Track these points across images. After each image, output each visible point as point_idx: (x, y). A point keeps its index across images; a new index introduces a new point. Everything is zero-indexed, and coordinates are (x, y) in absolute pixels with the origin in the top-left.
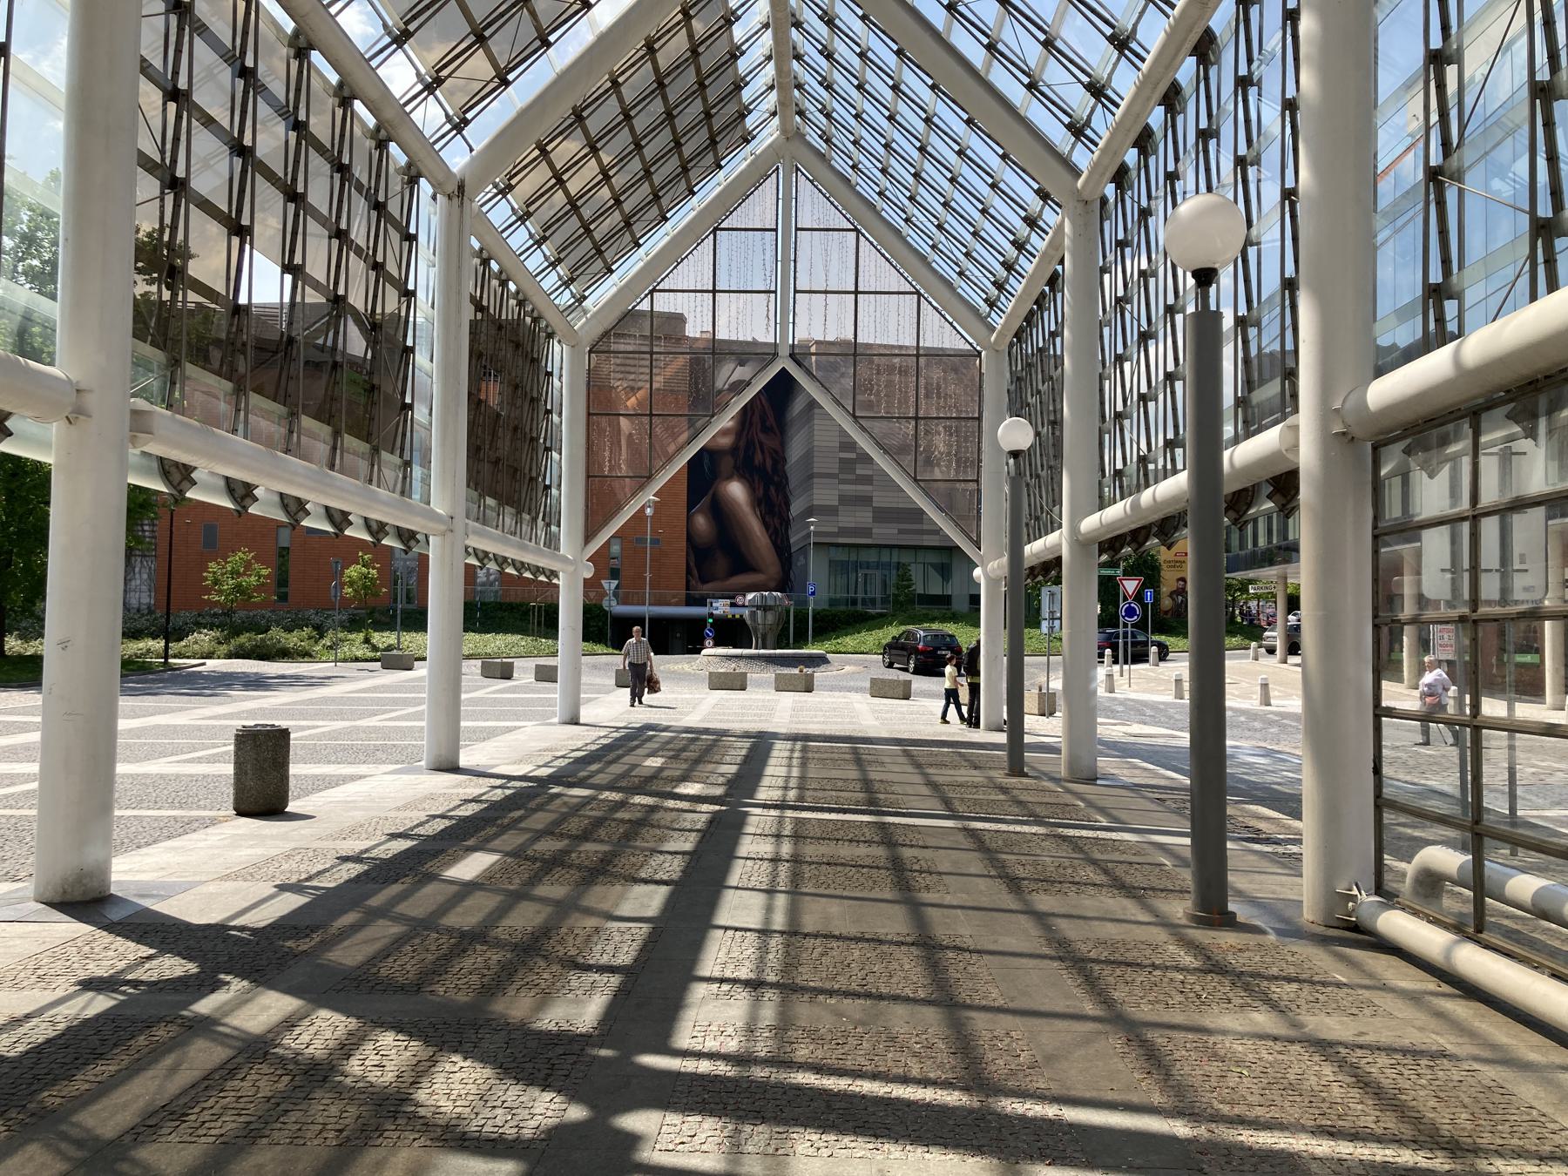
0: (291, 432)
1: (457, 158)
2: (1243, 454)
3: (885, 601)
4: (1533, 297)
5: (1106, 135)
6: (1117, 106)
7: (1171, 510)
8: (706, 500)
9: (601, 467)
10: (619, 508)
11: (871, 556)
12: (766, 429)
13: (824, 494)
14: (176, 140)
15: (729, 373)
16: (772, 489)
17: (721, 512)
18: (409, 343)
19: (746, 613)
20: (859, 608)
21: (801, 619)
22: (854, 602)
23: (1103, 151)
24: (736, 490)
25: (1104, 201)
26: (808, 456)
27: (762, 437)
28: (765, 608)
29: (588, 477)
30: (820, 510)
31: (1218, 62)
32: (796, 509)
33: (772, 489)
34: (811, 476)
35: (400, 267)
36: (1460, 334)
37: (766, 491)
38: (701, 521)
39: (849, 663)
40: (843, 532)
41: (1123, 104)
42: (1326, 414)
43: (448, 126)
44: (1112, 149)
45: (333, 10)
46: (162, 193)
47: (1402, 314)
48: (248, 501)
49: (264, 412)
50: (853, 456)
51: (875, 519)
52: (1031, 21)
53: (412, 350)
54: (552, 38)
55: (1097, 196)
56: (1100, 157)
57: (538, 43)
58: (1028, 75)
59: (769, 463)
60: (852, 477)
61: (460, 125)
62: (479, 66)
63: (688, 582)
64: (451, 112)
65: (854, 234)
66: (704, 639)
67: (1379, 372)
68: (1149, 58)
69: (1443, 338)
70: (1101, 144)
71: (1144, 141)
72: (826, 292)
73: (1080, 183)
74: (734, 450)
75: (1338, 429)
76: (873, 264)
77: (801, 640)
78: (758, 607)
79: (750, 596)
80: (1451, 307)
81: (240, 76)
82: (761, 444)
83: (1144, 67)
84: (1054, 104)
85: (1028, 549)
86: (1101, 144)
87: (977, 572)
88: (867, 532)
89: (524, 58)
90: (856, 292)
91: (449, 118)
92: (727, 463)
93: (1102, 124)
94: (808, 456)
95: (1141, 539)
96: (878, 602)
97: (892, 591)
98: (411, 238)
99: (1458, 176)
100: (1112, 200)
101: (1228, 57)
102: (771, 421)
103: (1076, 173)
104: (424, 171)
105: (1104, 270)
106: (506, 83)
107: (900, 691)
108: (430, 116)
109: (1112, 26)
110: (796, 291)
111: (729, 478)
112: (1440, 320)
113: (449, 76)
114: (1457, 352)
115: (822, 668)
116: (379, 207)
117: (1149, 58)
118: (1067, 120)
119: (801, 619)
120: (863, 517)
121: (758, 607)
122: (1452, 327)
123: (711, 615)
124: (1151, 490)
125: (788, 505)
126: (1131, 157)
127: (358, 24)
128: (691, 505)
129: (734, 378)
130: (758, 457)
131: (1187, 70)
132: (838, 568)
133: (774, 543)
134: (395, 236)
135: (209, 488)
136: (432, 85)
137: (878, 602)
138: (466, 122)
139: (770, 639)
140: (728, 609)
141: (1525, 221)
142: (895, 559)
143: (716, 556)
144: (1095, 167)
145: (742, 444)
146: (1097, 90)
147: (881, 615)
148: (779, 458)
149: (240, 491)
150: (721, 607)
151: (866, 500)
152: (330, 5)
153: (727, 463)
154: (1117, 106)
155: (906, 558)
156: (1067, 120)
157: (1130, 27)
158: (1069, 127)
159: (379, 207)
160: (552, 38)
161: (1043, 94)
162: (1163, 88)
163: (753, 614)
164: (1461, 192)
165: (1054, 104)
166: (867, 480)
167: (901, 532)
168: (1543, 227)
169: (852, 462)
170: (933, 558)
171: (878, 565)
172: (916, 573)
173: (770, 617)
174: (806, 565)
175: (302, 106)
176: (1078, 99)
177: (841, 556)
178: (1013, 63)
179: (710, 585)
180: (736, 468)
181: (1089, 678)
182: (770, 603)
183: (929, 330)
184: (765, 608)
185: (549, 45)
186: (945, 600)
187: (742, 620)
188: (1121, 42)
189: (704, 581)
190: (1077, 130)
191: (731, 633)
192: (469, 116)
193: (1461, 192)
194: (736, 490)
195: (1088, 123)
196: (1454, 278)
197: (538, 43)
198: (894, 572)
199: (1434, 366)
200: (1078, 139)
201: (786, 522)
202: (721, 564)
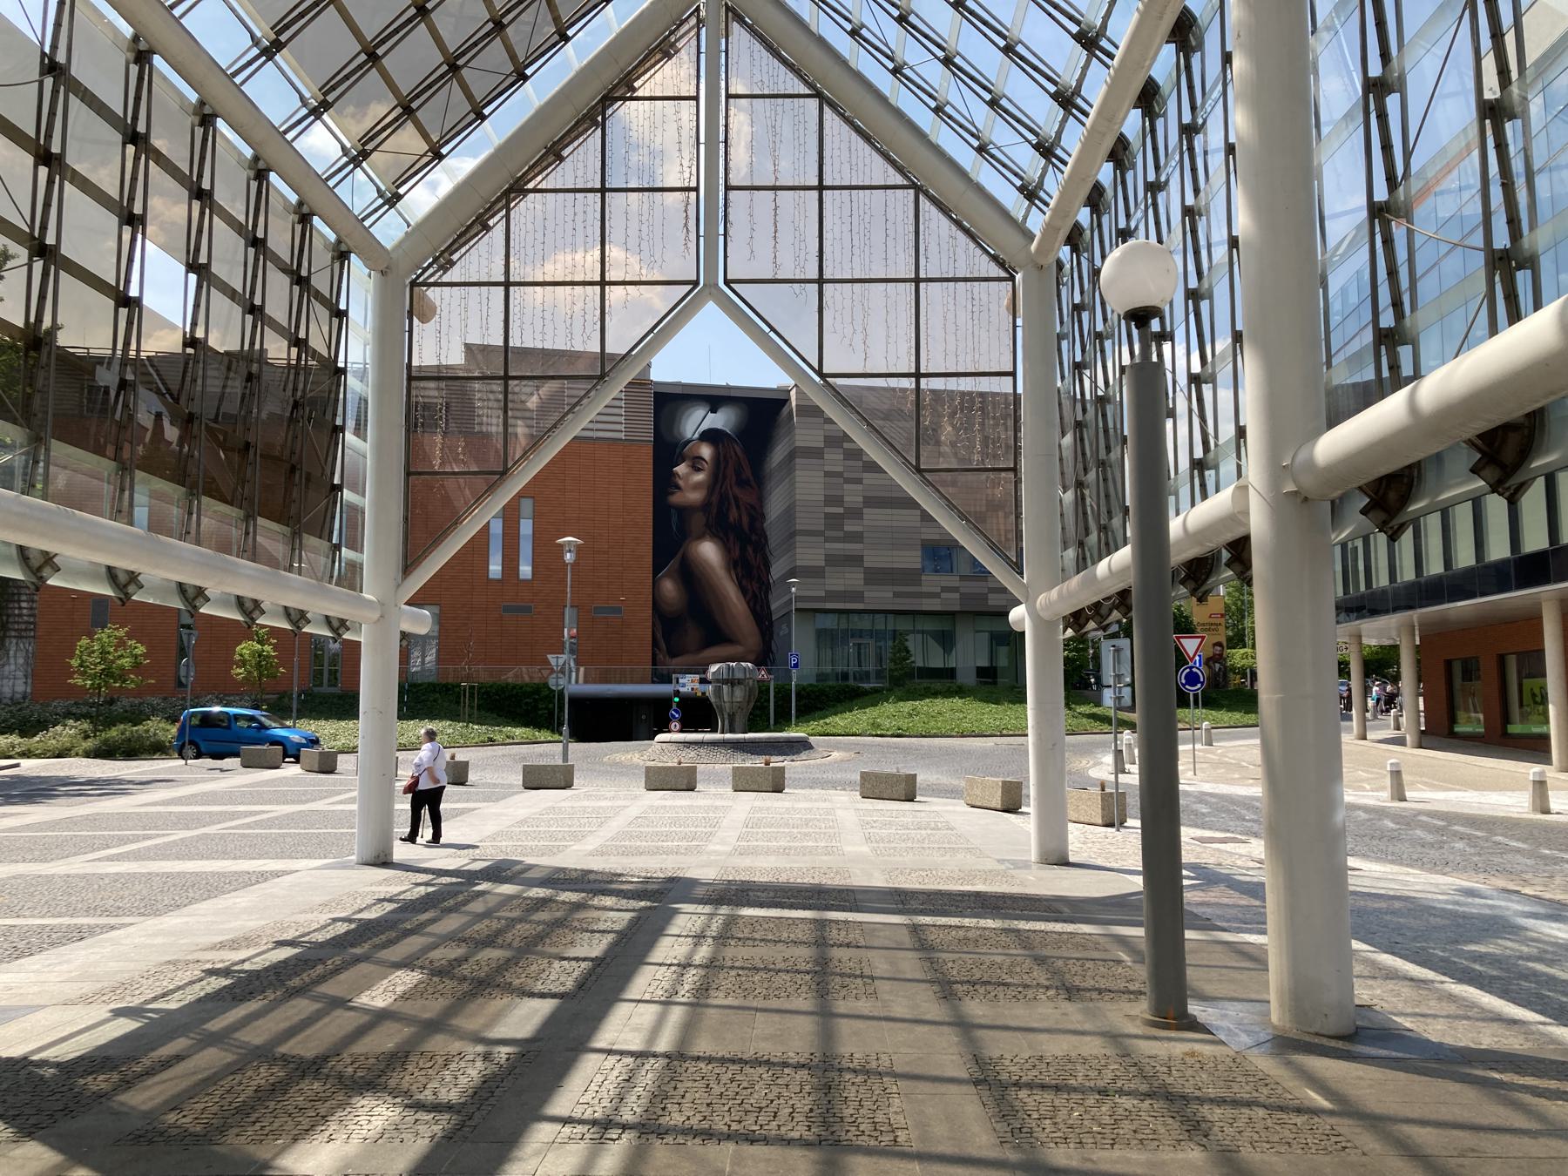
0: (247, 533)
1: (389, 230)
2: (1189, 521)
3: (879, 675)
4: (1493, 330)
5: (1056, 194)
6: (1065, 163)
7: (1514, 411)
8: (674, 563)
9: (427, 459)
10: (455, 522)
11: (864, 623)
12: (742, 483)
13: (809, 554)
14: (48, 203)
15: (696, 421)
16: (750, 549)
17: (691, 576)
18: (339, 422)
19: (709, 689)
20: (851, 682)
21: (783, 695)
22: (845, 676)
23: (1055, 211)
24: (709, 551)
25: (1060, 265)
26: (789, 513)
27: (737, 491)
28: (733, 683)
29: (408, 474)
30: (804, 571)
31: (1200, 47)
32: (776, 571)
33: (750, 549)
34: (793, 534)
35: (329, 348)
36: (1417, 376)
37: (743, 550)
38: (669, 587)
39: (837, 747)
40: (831, 595)
41: (1071, 161)
42: (1277, 470)
43: (380, 201)
44: (1062, 210)
45: (177, 12)
46: (30, 259)
47: (1355, 360)
48: (256, 613)
49: (215, 515)
50: (841, 510)
51: (867, 582)
52: (985, 24)
53: (342, 429)
54: (486, 111)
55: (1051, 260)
56: (1051, 218)
57: (472, 116)
58: (978, 138)
59: (745, 520)
60: (841, 534)
61: (393, 200)
62: (408, 140)
63: (654, 655)
64: (348, 145)
65: (814, 103)
66: (669, 721)
67: (1333, 421)
68: (1092, 112)
69: (1397, 383)
70: (1052, 203)
71: (1119, 154)
72: (775, 188)
73: (1033, 247)
74: (705, 506)
75: (1290, 487)
76: (845, 146)
77: (783, 721)
78: (725, 682)
79: (714, 668)
80: (1405, 352)
81: (198, 198)
82: (736, 499)
83: (1088, 122)
84: (1004, 167)
85: (1175, 526)
86: (1052, 203)
87: (1017, 614)
88: (859, 596)
89: (455, 132)
90: (821, 188)
91: (380, 194)
92: (698, 521)
93: (1073, 140)
94: (789, 513)
95: (1509, 454)
96: (873, 675)
97: (887, 665)
98: (342, 315)
99: (1406, 213)
100: (1068, 266)
101: (1172, 106)
102: (748, 473)
103: (1030, 236)
104: (219, 110)
105: (1060, 337)
106: (439, 157)
107: (901, 789)
108: (359, 191)
109: (1021, 178)
110: (728, 188)
111: (701, 537)
112: (1394, 367)
113: (375, 149)
114: (1412, 394)
115: (803, 755)
116: (301, 282)
117: (1092, 112)
118: (1074, 29)
119: (783, 695)
120: (851, 579)
121: (725, 682)
122: (1407, 370)
123: (677, 693)
124: (1105, 562)
125: (767, 566)
126: (1106, 174)
127: (219, 31)
128: (657, 567)
129: (704, 427)
130: (733, 514)
131: (1132, 123)
132: (826, 638)
133: (753, 611)
134: (321, 312)
135: (274, 616)
136: (358, 157)
137: (873, 675)
138: (399, 197)
139: (740, 720)
140: (697, 685)
141: (1479, 260)
142: (890, 627)
143: (687, 626)
144: (1049, 229)
145: (715, 499)
146: (1046, 150)
147: (876, 691)
148: (757, 514)
149: (294, 616)
150: (688, 684)
151: (857, 560)
152: (172, 7)
153: (698, 521)
154: (1065, 163)
155: (903, 625)
156: (1074, 29)
157: (1099, 23)
158: (1021, 189)
159: (301, 282)
160: (486, 111)
161: (992, 156)
162: (1108, 143)
163: (718, 692)
164: (1410, 233)
165: (1004, 167)
166: (857, 537)
167: (896, 595)
168: (1386, 336)
169: (841, 517)
170: (930, 625)
171: (871, 633)
172: (913, 643)
173: (739, 693)
174: (790, 634)
175: (305, 264)
176: (1028, 161)
177: (829, 622)
178: (961, 126)
179: (675, 661)
180: (707, 525)
181: (1330, 767)
182: (738, 675)
183: (933, 248)
184: (733, 683)
185: (483, 118)
186: (950, 673)
187: (704, 700)
188: (1089, 40)
189: (673, 654)
190: (1030, 193)
191: (698, 714)
192: (401, 191)
193: (1410, 233)
194: (709, 551)
195: (1077, 91)
196: (1408, 322)
197: (472, 116)
198: (890, 643)
199: (1389, 412)
200: (1049, 161)
201: (765, 586)
202: (693, 634)
